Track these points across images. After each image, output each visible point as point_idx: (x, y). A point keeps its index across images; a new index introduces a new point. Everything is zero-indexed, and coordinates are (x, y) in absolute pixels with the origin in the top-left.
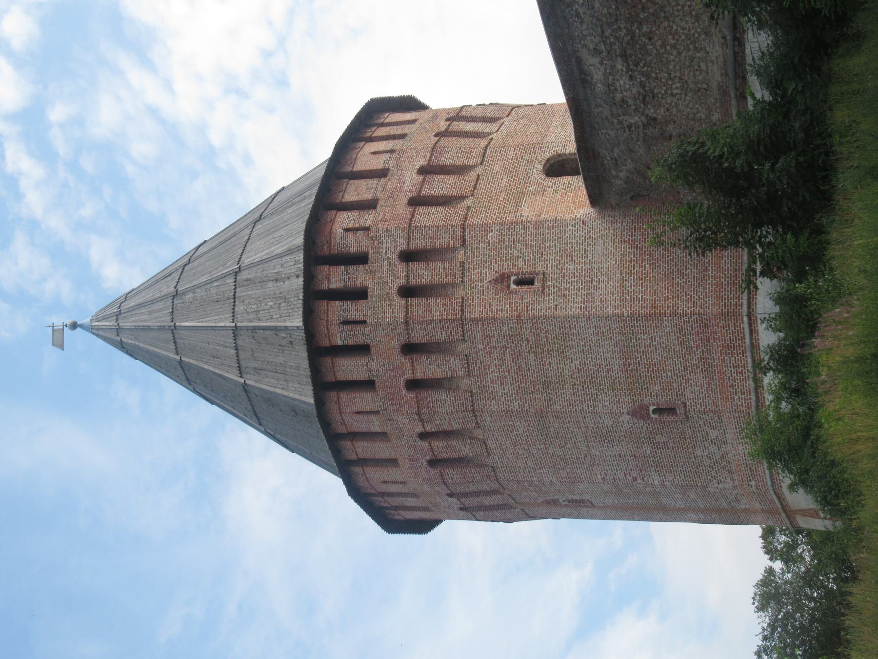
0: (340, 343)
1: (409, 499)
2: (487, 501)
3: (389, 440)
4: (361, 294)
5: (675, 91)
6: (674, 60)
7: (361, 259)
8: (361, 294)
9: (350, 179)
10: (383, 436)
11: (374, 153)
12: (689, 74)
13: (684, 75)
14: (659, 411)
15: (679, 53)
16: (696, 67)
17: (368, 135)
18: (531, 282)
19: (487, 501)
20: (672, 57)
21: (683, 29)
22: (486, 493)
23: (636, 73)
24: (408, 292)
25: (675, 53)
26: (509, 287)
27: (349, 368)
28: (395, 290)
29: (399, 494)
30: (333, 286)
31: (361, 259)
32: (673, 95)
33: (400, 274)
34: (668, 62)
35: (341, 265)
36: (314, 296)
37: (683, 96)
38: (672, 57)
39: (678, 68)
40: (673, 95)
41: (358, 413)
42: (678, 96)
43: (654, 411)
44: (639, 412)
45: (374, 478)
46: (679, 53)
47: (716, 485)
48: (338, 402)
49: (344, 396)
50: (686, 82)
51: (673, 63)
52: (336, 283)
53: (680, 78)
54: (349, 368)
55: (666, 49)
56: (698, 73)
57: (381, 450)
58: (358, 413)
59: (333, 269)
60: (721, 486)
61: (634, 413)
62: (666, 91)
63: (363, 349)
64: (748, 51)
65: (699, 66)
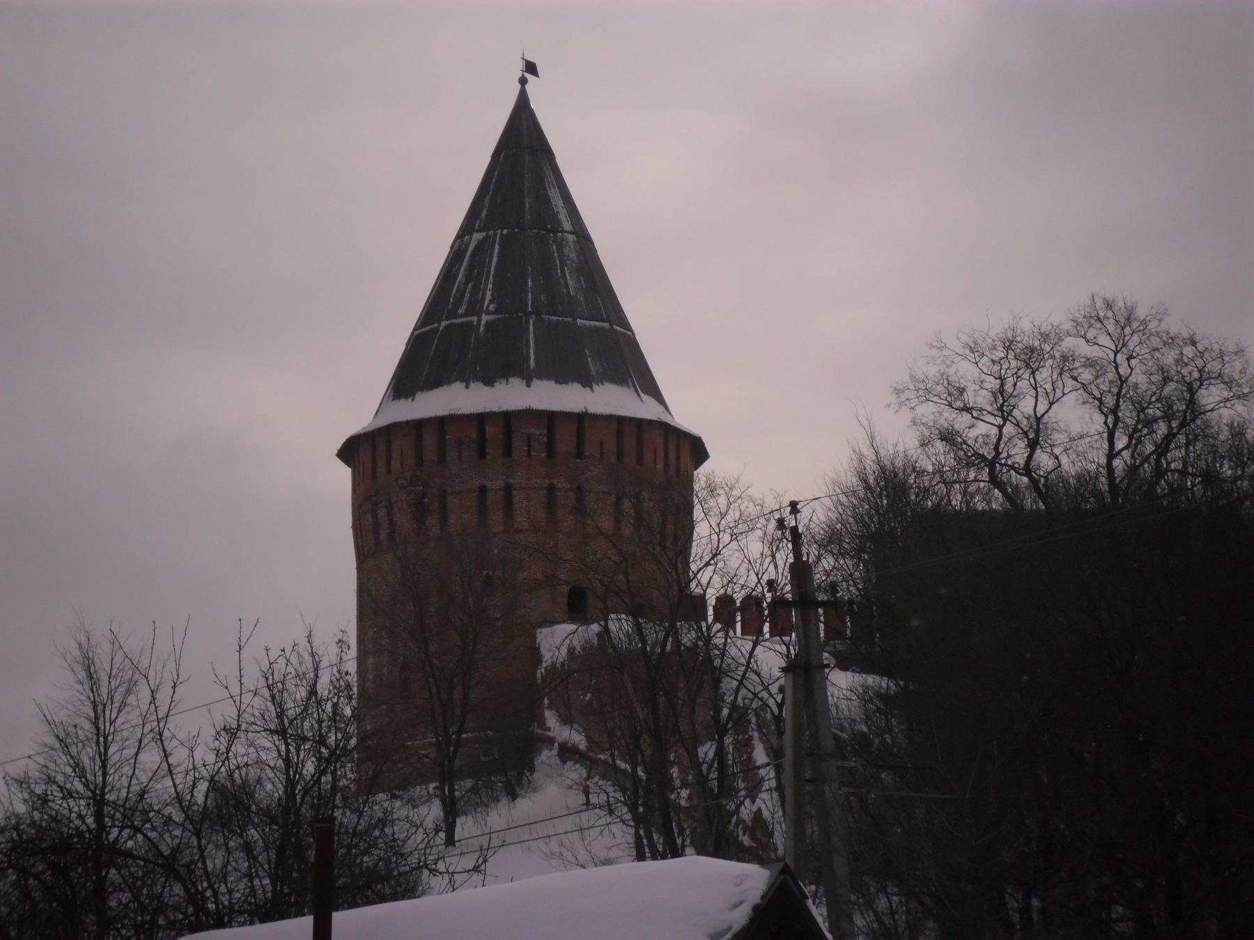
31: (508, 451)
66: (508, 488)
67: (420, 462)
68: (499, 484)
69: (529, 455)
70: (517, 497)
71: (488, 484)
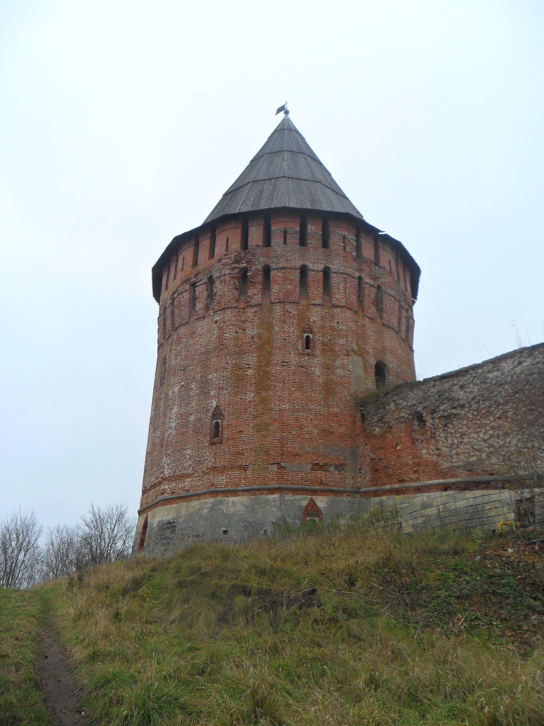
0: (272, 229)
1: (173, 276)
2: (169, 322)
3: (210, 258)
4: (303, 242)
5: (449, 439)
6: (479, 436)
7: (325, 244)
8: (303, 242)
9: (375, 245)
10: (212, 254)
11: (390, 262)
12: (465, 448)
13: (465, 445)
14: (217, 425)
15: (485, 441)
16: (472, 454)
17: (399, 261)
18: (307, 347)
19: (169, 322)
20: (481, 435)
21: (509, 443)
22: (173, 320)
23: (467, 410)
24: (304, 271)
25: (486, 437)
26: (305, 332)
27: (256, 235)
28: (306, 263)
29: (176, 268)
30: (309, 226)
31: (325, 244)
32: (446, 438)
33: (316, 266)
34: (477, 433)
35: (323, 232)
36: (303, 216)
37: (446, 445)
38: (481, 435)
39: (472, 440)
40: (446, 438)
41: (228, 240)
42: (445, 441)
43: (217, 423)
44: (217, 413)
45: (187, 254)
46: (485, 441)
47: (167, 462)
48: (235, 228)
49: (239, 231)
50: (458, 447)
51: (476, 436)
52: (311, 228)
53: (461, 442)
54: (256, 235)
55: (489, 430)
56: (467, 455)
57: (203, 255)
58: (228, 240)
59: (320, 228)
60: (166, 465)
61: (217, 407)
62: (450, 432)
63: (267, 243)
64: (493, 491)
65: (472, 456)
66: (326, 272)
67: (245, 245)
68: (321, 267)
69: (345, 249)
70: (335, 279)
71: (310, 266)
